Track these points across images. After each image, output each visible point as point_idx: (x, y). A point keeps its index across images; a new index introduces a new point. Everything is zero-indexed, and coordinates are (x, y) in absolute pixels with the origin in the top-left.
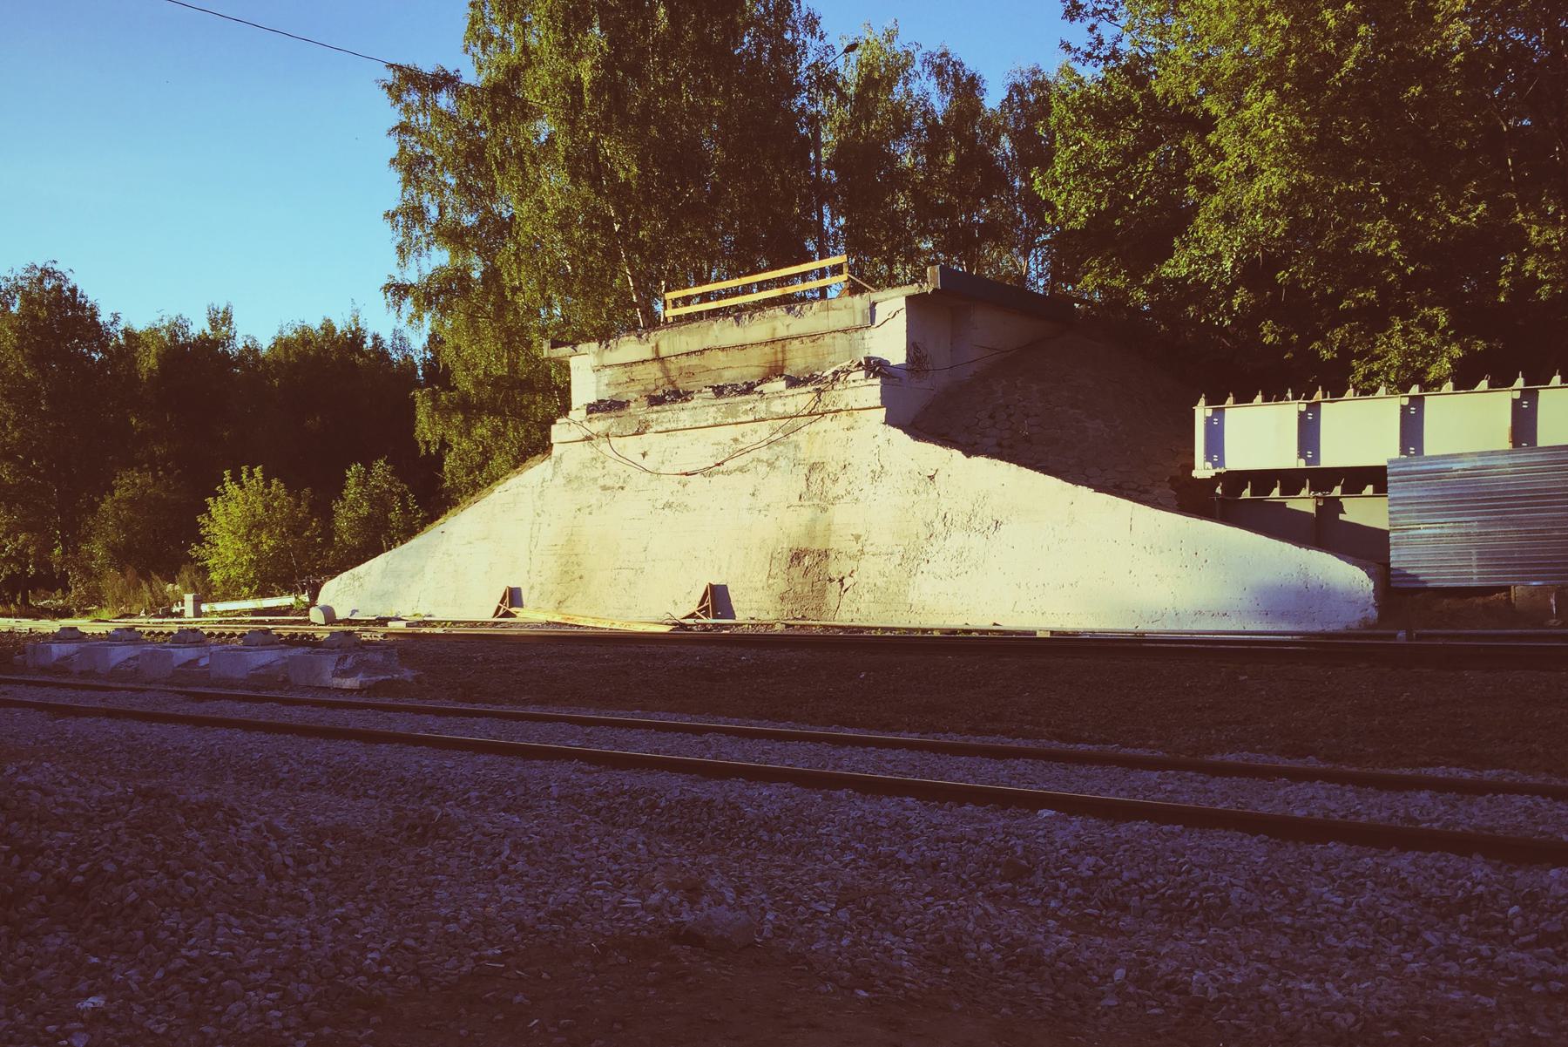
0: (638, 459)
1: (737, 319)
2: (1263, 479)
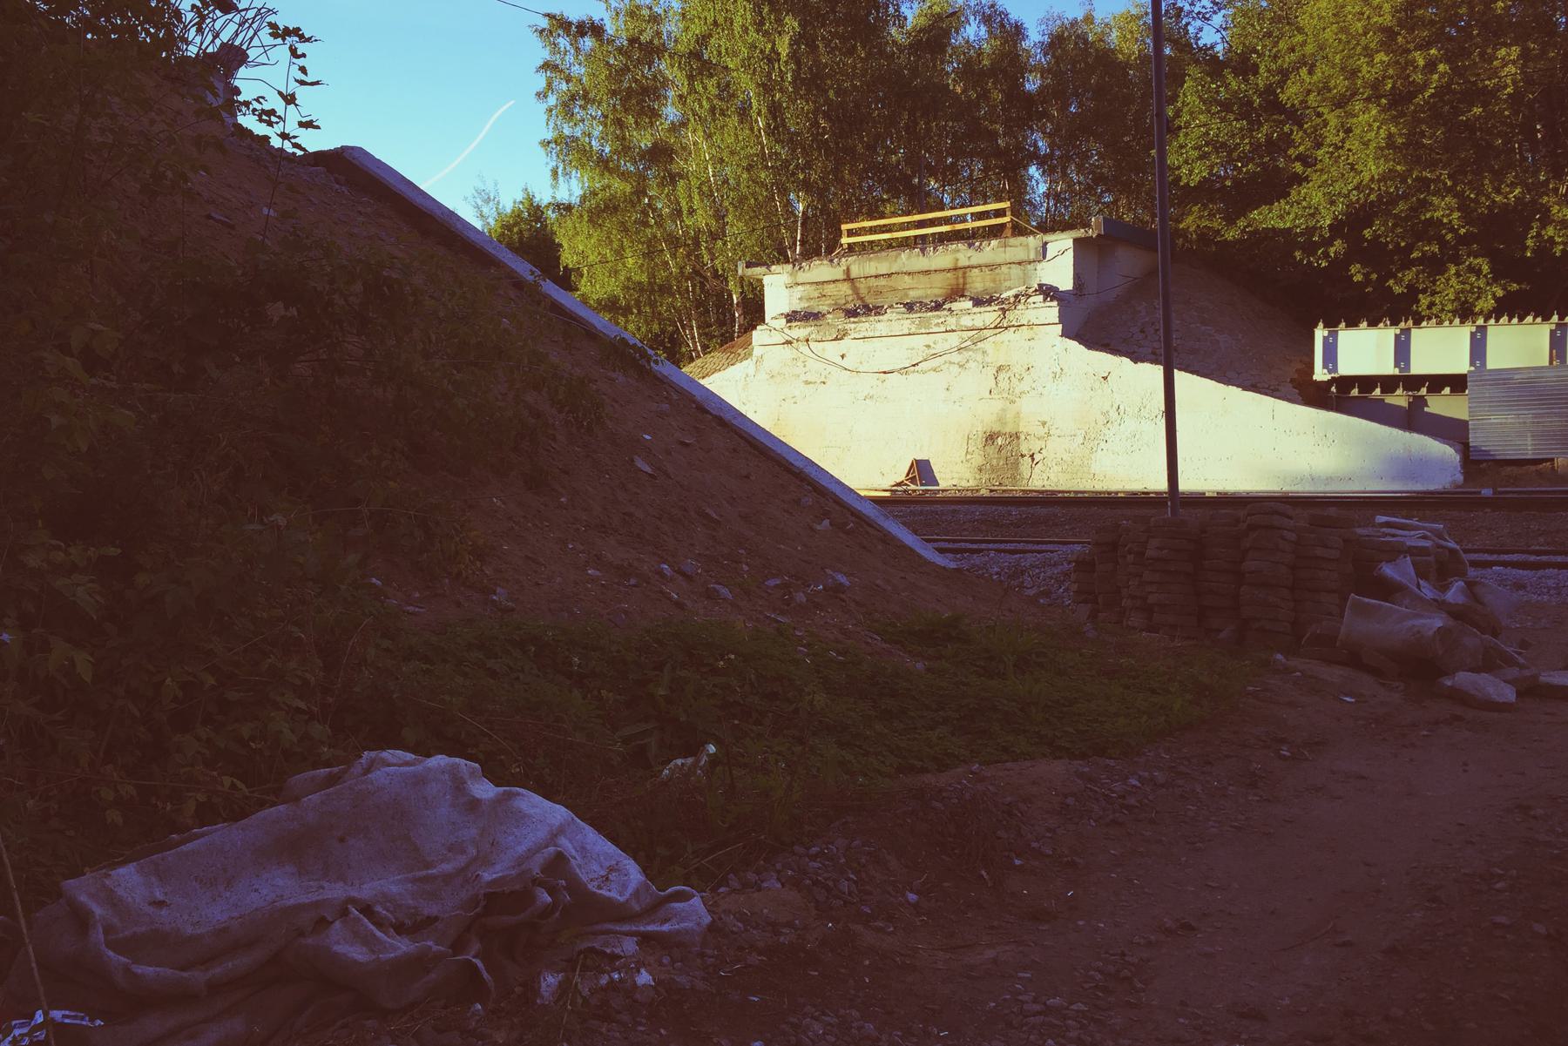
0: (838, 360)
1: (923, 250)
2: (1367, 382)
